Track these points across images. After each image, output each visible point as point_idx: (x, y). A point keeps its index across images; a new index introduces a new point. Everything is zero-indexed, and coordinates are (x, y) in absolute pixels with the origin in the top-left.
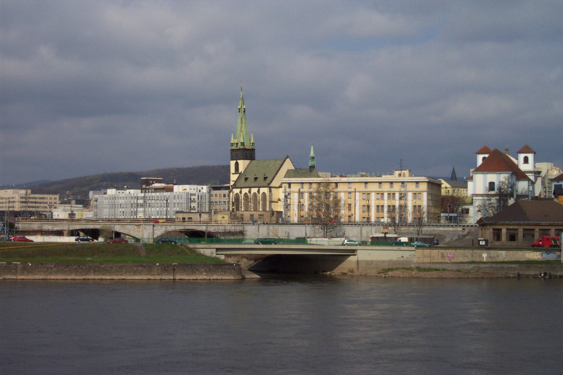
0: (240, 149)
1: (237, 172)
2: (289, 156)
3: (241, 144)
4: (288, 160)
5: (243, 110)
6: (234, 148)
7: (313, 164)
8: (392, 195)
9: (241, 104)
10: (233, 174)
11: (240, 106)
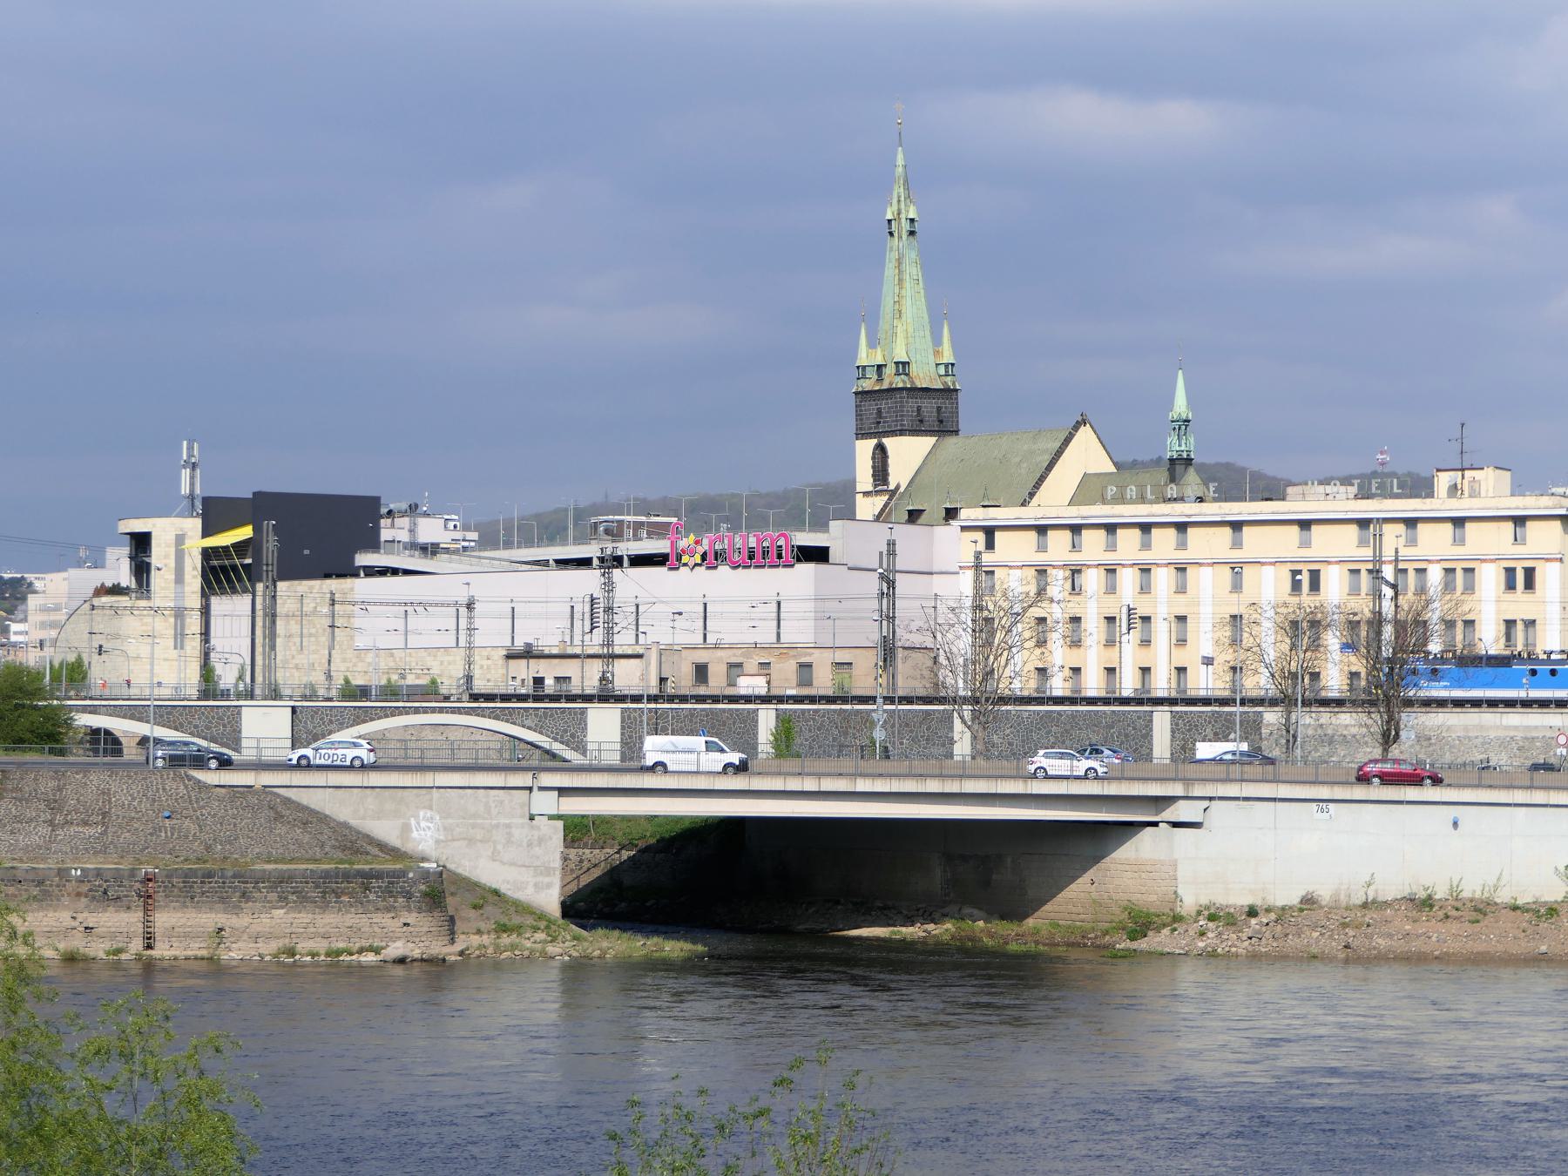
0: (891, 390)
1: (880, 488)
2: (1090, 417)
3: (897, 370)
4: (1085, 433)
5: (906, 226)
6: (867, 385)
7: (1183, 448)
8: (1459, 574)
9: (899, 201)
10: (866, 494)
11: (895, 207)
